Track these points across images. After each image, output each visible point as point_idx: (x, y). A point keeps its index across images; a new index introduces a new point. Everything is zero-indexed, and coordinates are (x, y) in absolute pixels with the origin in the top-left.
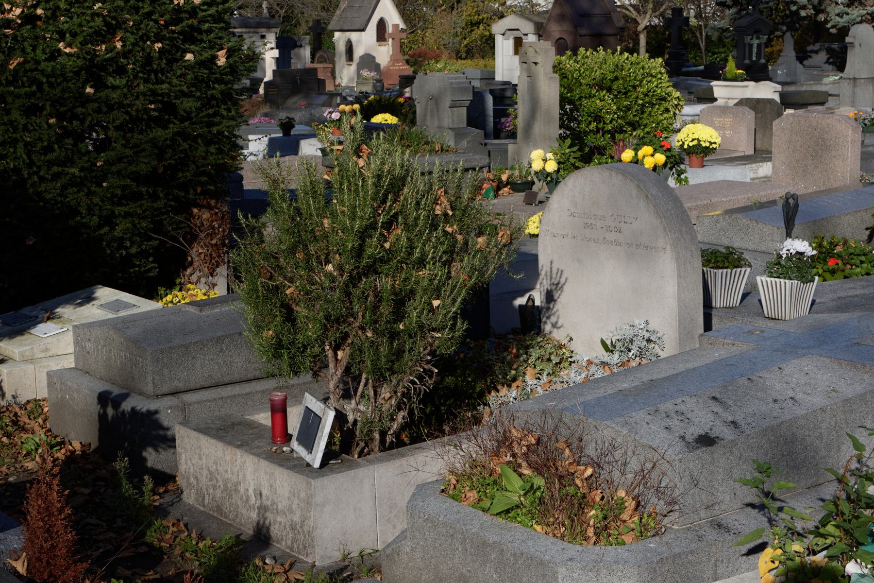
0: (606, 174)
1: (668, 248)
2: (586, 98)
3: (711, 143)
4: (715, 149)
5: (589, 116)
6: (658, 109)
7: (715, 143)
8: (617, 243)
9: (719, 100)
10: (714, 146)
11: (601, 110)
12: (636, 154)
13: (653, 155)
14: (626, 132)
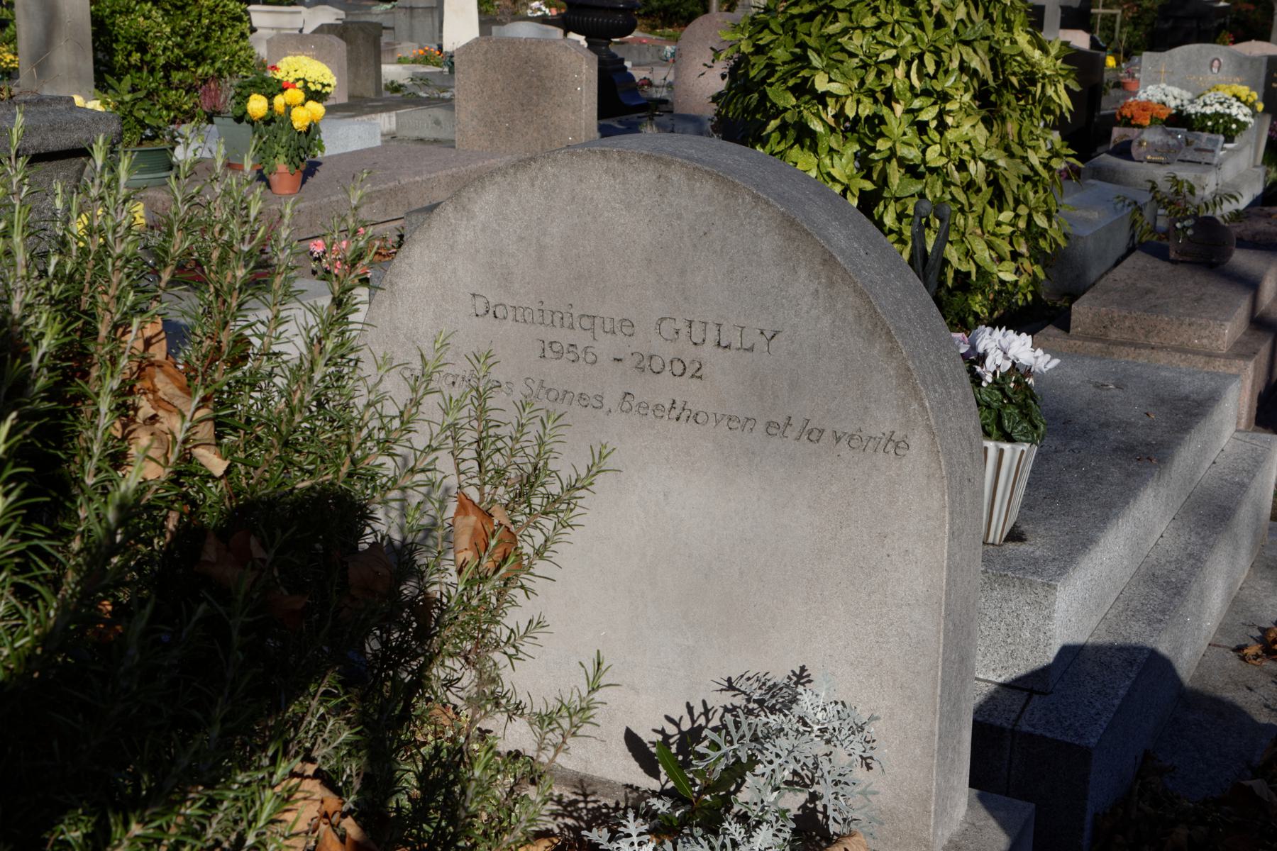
0: (644, 177)
1: (918, 440)
2: (121, 13)
3: (324, 86)
4: (327, 93)
5: (128, 43)
6: (232, 33)
7: (329, 85)
8: (679, 412)
9: (259, 31)
10: (328, 89)
11: (147, 33)
12: (271, 104)
13: (303, 105)
14: (186, 68)
